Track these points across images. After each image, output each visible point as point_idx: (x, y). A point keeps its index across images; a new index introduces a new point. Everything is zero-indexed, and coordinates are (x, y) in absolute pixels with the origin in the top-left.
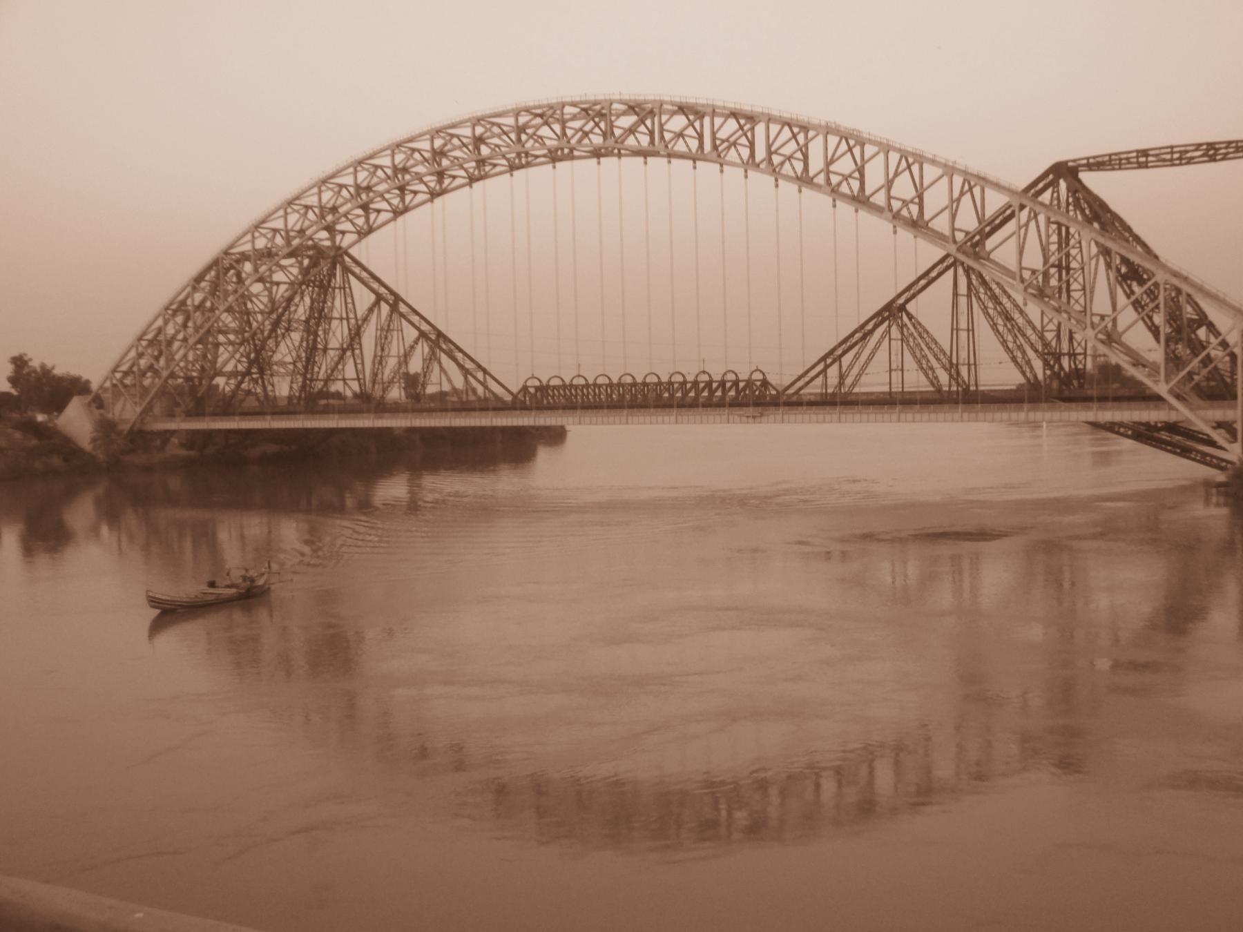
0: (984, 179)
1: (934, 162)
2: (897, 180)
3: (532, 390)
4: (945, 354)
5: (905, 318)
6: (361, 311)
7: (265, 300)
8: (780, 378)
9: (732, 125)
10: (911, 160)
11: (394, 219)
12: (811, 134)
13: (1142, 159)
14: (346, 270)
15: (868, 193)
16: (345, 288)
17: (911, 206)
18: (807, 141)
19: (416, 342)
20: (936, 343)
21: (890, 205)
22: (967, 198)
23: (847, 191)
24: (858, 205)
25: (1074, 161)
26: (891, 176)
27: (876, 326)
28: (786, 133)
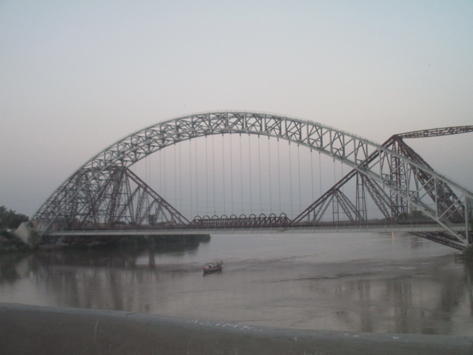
1: (348, 135)
3: (197, 221)
4: (354, 207)
5: (339, 193)
6: (133, 190)
9: (273, 121)
12: (302, 125)
13: (426, 133)
14: (127, 175)
16: (127, 182)
18: (301, 127)
19: (153, 202)
21: (356, 162)
26: (357, 147)
27: (328, 196)
28: (293, 124)
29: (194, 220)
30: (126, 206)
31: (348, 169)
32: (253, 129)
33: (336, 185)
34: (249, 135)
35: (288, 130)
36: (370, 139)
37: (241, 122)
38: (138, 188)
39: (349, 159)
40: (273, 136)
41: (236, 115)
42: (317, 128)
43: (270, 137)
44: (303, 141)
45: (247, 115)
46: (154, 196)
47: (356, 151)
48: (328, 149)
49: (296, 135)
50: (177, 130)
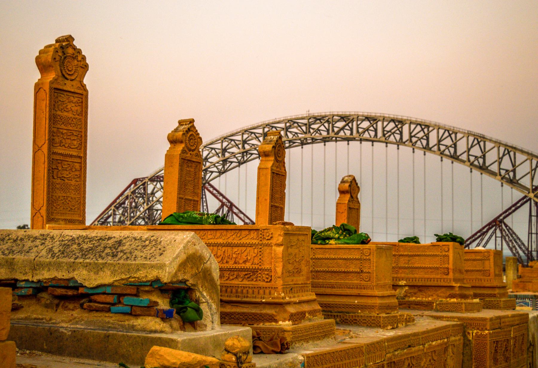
0: (515, 148)
1: (490, 140)
4: (524, 245)
9: (392, 125)
10: (479, 140)
11: (219, 176)
12: (431, 129)
15: (458, 154)
17: (450, 148)
18: (429, 132)
20: (520, 239)
21: (500, 172)
22: (506, 158)
23: (449, 154)
24: (453, 160)
26: (501, 155)
28: (419, 128)
31: (518, 195)
32: (366, 135)
33: (501, 215)
34: (361, 143)
35: (413, 134)
36: (519, 145)
37: (349, 127)
38: (222, 206)
39: (492, 170)
40: (391, 143)
41: (343, 118)
42: (451, 132)
43: (388, 145)
44: (459, 156)
45: (359, 117)
46: (243, 218)
47: (500, 160)
48: (464, 157)
49: (395, 135)
50: (223, 155)
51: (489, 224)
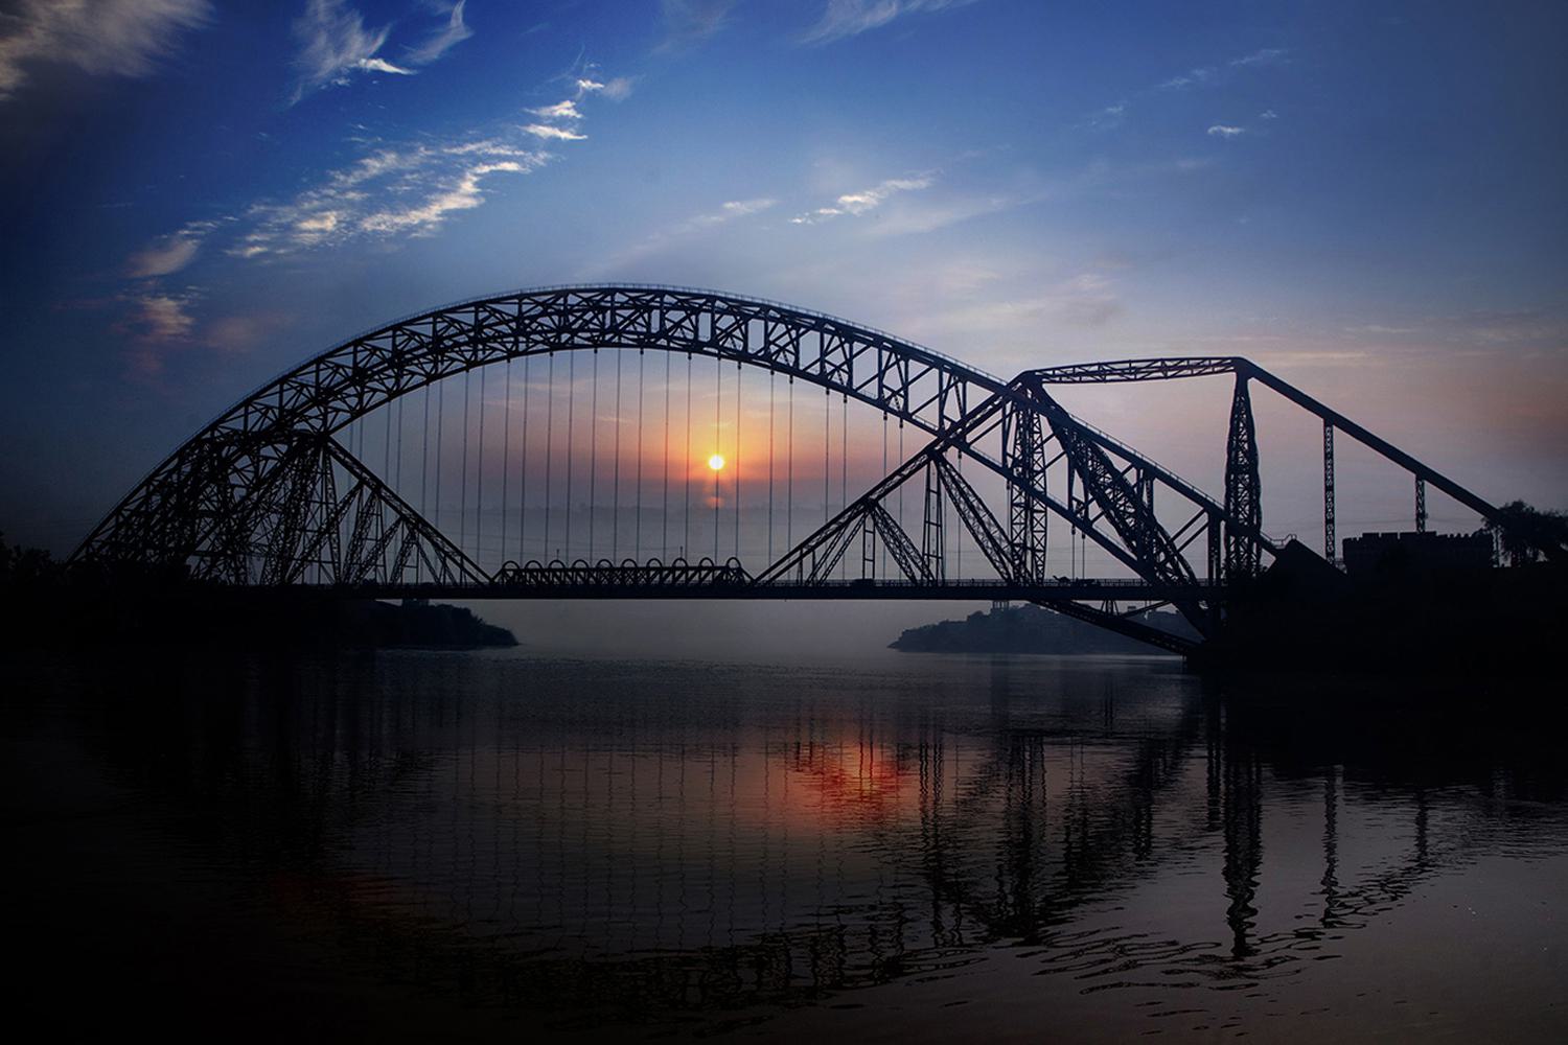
2: (888, 372)
6: (342, 494)
7: (250, 476)
8: (754, 567)
13: (1101, 373)
14: (328, 452)
16: (327, 472)
19: (397, 524)
25: (1040, 371)
27: (851, 519)
29: (503, 572)
30: (320, 533)
35: (771, 339)
38: (359, 487)
51: (853, 506)
